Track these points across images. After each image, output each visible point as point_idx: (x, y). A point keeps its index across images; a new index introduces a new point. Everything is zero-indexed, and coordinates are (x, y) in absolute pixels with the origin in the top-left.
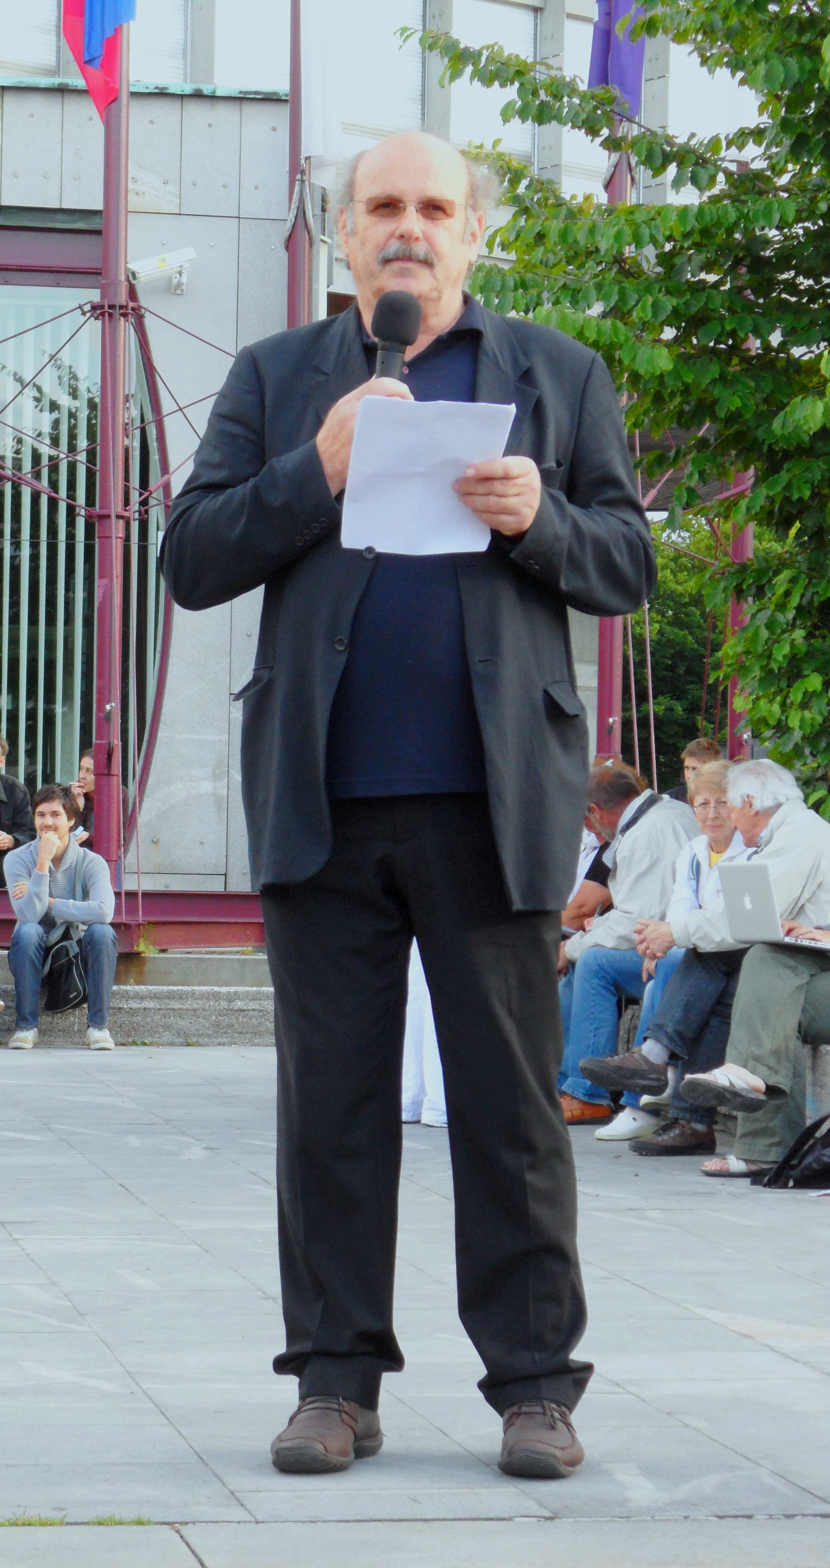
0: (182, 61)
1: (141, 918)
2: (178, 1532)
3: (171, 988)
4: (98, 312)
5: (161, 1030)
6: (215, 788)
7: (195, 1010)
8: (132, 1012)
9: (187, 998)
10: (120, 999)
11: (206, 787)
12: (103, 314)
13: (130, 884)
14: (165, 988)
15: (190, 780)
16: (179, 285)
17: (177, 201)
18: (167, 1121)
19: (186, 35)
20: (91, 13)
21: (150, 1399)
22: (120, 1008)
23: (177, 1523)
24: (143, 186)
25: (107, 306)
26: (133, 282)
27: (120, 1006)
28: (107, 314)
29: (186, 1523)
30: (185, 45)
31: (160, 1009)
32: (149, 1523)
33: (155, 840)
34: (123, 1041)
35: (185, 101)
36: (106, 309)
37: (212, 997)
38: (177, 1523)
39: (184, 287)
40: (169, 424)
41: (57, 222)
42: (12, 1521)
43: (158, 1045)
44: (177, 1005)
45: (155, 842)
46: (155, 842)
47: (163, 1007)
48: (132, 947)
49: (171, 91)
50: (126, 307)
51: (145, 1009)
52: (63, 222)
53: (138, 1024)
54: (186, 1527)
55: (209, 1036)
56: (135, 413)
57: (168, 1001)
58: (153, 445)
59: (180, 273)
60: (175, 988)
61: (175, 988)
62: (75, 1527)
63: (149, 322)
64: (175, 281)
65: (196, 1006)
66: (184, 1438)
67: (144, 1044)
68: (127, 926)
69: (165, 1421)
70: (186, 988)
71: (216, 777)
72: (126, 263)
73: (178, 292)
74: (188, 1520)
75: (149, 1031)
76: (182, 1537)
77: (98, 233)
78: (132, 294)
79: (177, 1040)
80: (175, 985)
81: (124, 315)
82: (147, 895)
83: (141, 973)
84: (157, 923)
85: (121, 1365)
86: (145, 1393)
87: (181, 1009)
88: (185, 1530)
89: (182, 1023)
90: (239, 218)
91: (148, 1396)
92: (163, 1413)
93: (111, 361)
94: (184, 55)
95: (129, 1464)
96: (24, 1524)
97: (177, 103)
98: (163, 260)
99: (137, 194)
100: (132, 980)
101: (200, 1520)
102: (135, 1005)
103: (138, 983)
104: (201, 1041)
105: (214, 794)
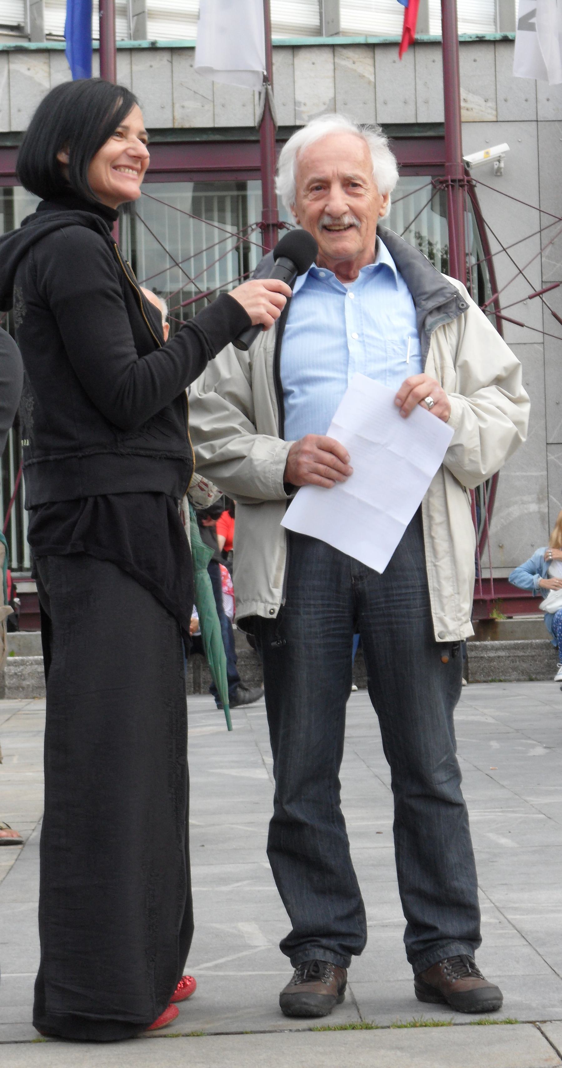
0: (494, 27)
1: (493, 596)
2: (539, 1029)
3: (516, 642)
4: (444, 185)
5: (510, 671)
6: (540, 508)
7: (533, 656)
8: (491, 660)
9: (527, 648)
10: (482, 651)
11: (533, 507)
12: (447, 186)
13: (485, 574)
14: (512, 642)
15: (522, 503)
16: (499, 169)
17: (494, 113)
18: (517, 731)
19: (496, 9)
20: (459, 271)
21: (514, 926)
22: (482, 657)
23: (538, 1022)
24: (472, 103)
25: (450, 181)
26: (467, 169)
27: (482, 655)
28: (450, 186)
29: (545, 1022)
30: (495, 16)
31: (509, 657)
32: (516, 1022)
33: (501, 545)
34: (485, 679)
35: (497, 46)
36: (450, 183)
37: (544, 647)
38: (538, 1022)
39: (502, 170)
40: (497, 261)
41: (415, 132)
42: (412, 1024)
43: (510, 681)
44: (521, 654)
45: (501, 547)
46: (501, 547)
47: (511, 655)
48: (489, 615)
49: (487, 38)
50: (463, 180)
51: (499, 657)
52: (419, 132)
53: (495, 668)
54: (545, 1024)
55: (543, 674)
56: (473, 260)
57: (514, 651)
58: (487, 276)
59: (499, 161)
60: (519, 642)
61: (519, 642)
62: (460, 1027)
63: (479, 191)
64: (496, 167)
65: (534, 653)
66: (539, 954)
67: (500, 681)
68: (484, 601)
69: (525, 943)
70: (526, 641)
71: (540, 501)
72: (462, 156)
73: (499, 174)
74: (546, 1019)
75: (502, 672)
76: (542, 1033)
77: (441, 138)
78: (467, 173)
79: (522, 677)
80: (518, 639)
81: (462, 186)
82: (495, 580)
83: (495, 633)
84: (505, 600)
85: (491, 902)
86: (509, 922)
87: (524, 656)
88: (544, 1027)
89: (525, 665)
90: (537, 121)
91: (512, 924)
92: (523, 937)
93: (455, 218)
94: (495, 22)
95: (499, 976)
96: (421, 1026)
97: (492, 47)
98: (487, 153)
99: (467, 109)
100: (489, 638)
101: (555, 1019)
102: (492, 654)
103: (493, 639)
104: (538, 677)
105: (539, 512)
